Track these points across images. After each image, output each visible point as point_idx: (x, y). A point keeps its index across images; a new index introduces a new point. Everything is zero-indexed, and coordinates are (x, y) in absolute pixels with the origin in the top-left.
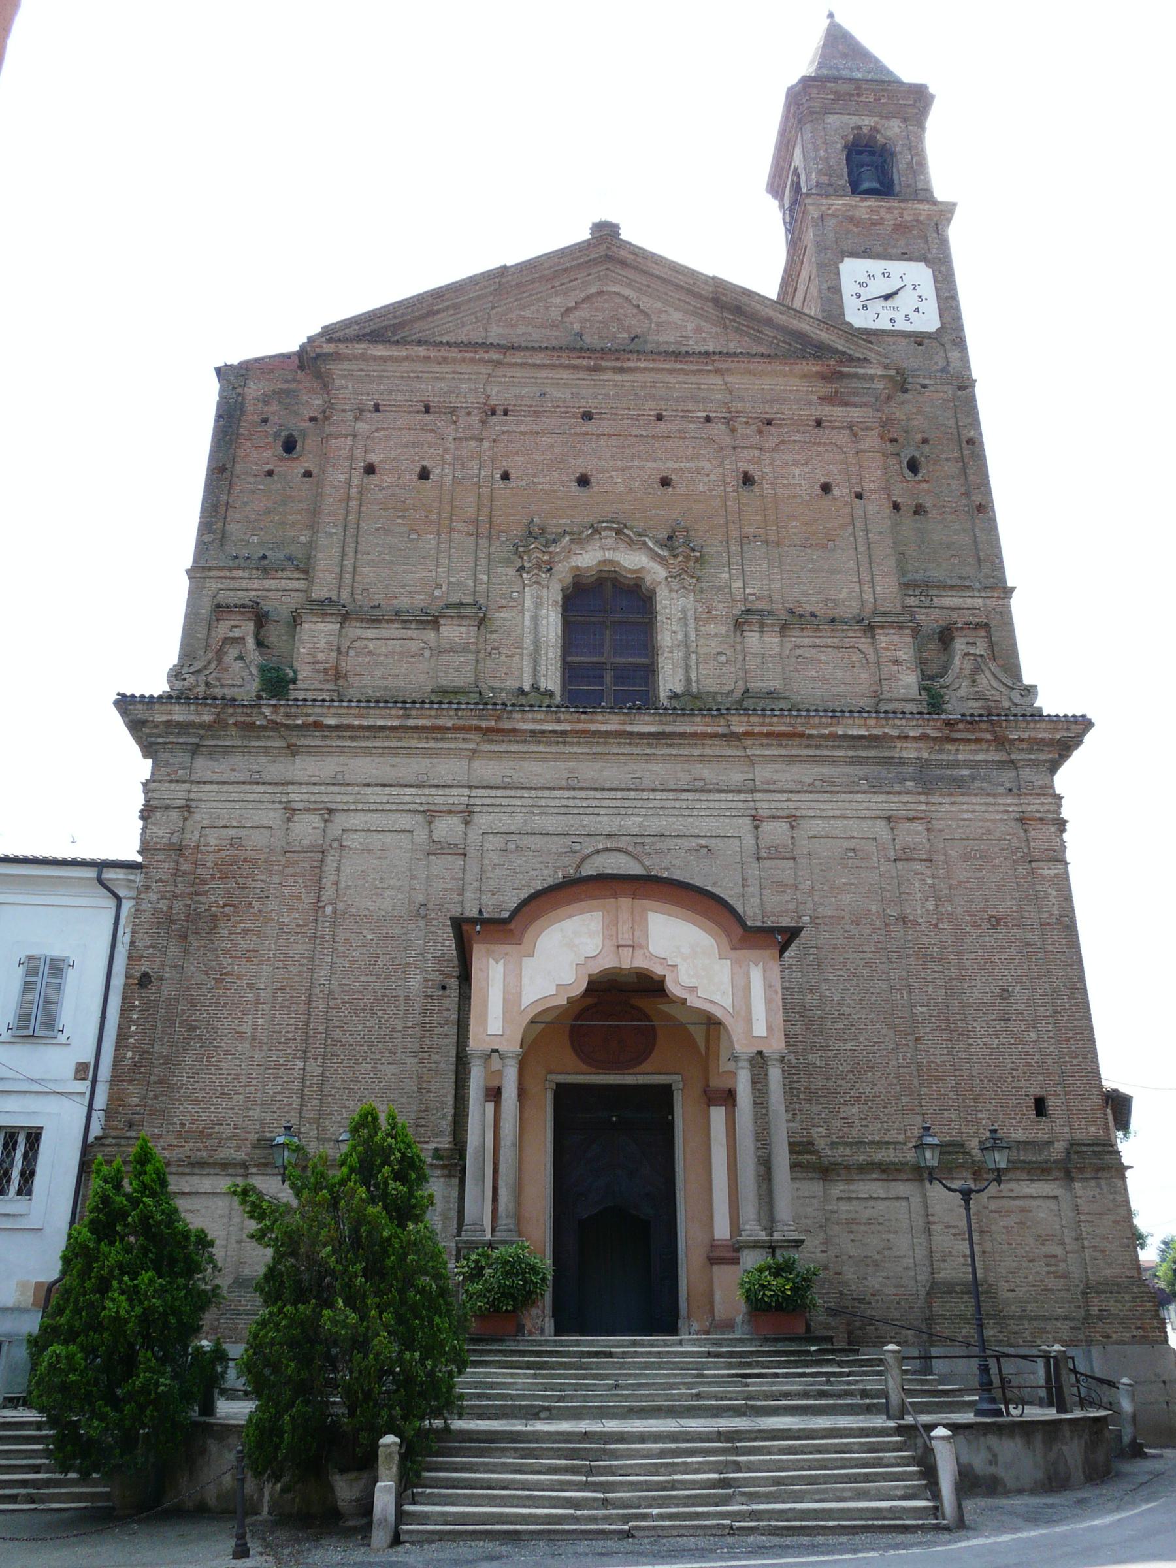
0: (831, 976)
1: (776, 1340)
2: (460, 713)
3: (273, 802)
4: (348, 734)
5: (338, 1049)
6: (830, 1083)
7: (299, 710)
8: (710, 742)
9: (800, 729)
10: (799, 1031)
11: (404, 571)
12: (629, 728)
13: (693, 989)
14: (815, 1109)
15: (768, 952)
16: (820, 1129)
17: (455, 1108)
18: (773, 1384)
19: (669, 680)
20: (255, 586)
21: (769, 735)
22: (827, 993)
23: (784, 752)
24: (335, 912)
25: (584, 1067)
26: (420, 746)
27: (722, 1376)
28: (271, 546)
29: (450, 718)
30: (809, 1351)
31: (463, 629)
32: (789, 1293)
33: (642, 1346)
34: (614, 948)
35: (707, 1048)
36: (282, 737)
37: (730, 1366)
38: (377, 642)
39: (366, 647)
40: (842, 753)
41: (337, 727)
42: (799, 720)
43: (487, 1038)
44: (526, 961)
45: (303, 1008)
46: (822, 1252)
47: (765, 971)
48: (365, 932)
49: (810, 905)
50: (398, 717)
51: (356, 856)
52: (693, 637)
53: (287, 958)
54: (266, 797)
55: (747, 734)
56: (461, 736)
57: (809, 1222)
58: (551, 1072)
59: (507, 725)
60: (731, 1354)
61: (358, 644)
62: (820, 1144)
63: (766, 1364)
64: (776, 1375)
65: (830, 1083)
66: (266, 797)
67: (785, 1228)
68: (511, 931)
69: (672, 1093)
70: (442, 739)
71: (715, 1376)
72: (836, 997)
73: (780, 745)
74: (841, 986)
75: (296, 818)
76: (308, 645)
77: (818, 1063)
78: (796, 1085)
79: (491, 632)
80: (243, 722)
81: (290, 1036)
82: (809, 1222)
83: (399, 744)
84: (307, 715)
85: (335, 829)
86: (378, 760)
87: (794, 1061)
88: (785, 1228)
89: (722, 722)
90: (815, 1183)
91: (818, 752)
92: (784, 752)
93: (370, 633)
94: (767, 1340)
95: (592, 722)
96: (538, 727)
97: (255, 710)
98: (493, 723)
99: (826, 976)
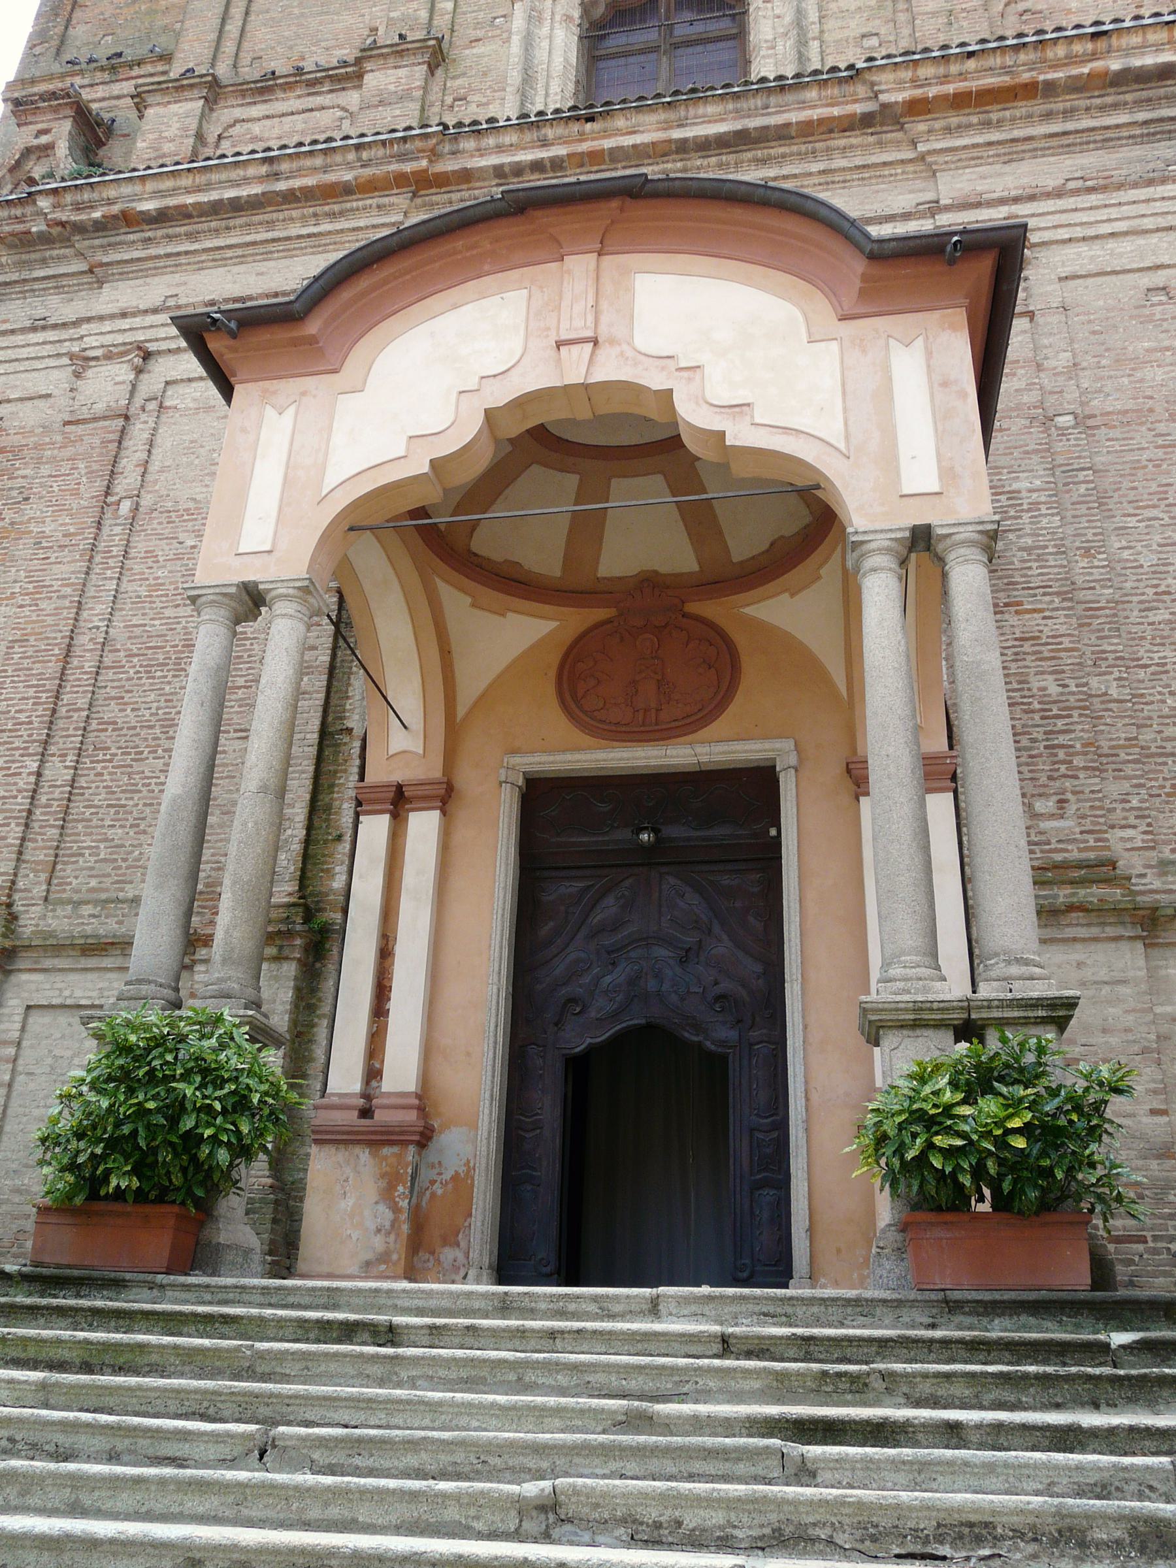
0: (1132, 522)
1: (992, 1309)
2: (365, 155)
3: (59, 355)
4: (182, 230)
5: (108, 737)
6: (1147, 736)
7: (95, 196)
8: (842, 142)
9: (1026, 77)
10: (1063, 630)
11: (321, 23)
12: (677, 134)
13: (741, 408)
14: (1114, 789)
15: (937, 314)
16: (1130, 833)
17: (310, 828)
18: (921, 1474)
19: (764, 67)
20: (99, 95)
21: (960, 101)
22: (1126, 554)
23: (995, 136)
24: (136, 508)
25: (587, 740)
26: (304, 231)
27: (727, 1426)
28: (130, 42)
29: (349, 166)
30: (1105, 1347)
31: (402, 72)
32: (1020, 1143)
33: (532, 1313)
34: (552, 352)
35: (850, 687)
36: (80, 254)
37: (782, 1388)
38: (268, 122)
39: (249, 131)
40: (1123, 118)
41: (161, 217)
42: (1023, 57)
43: (237, 562)
44: (347, 404)
45: (53, 668)
46: (1154, 1112)
47: (929, 354)
48: (182, 536)
49: (1072, 394)
50: (261, 179)
51: (185, 420)
52: (813, 16)
53: (40, 587)
54: (48, 350)
55: (917, 107)
56: (373, 202)
57: (1114, 1040)
58: (514, 752)
59: (449, 165)
60: (807, 1347)
61: (237, 130)
62: (1132, 863)
63: (926, 1388)
64: (953, 1433)
65: (1147, 736)
66: (48, 350)
67: (1014, 970)
68: (312, 340)
69: (776, 781)
70: (342, 213)
71: (698, 1424)
72: (1148, 560)
73: (987, 124)
74: (1157, 538)
75: (90, 373)
76: (151, 136)
77: (1114, 692)
78: (1062, 739)
79: (453, 78)
80: (12, 234)
81: (23, 717)
82: (1114, 1040)
83: (270, 235)
84: (110, 202)
85: (151, 383)
86: (236, 269)
87: (1054, 690)
88: (1014, 970)
89: (861, 90)
90: (1124, 946)
91: (1070, 126)
92: (995, 136)
93: (256, 111)
94: (952, 1307)
95: (606, 134)
96: (505, 159)
97: (29, 210)
98: (424, 163)
99: (1119, 521)
